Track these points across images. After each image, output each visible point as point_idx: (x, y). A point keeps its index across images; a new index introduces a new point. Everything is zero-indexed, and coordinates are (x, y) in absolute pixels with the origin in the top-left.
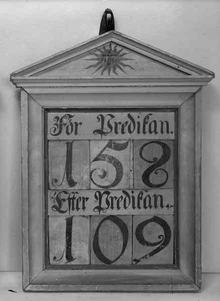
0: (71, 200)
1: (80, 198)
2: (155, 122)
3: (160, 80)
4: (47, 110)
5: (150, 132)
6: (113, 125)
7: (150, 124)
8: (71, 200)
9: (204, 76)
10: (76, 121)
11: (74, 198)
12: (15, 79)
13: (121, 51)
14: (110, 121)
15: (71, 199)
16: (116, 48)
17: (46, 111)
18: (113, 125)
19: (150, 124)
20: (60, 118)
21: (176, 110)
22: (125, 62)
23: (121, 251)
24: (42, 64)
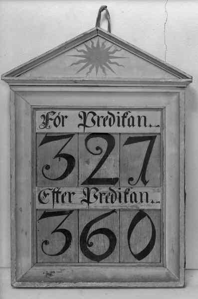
0: (55, 194)
1: (66, 193)
2: (133, 117)
3: (166, 83)
4: (35, 109)
5: (129, 125)
6: (96, 121)
7: (129, 120)
8: (55, 194)
9: (184, 80)
10: (63, 115)
11: (58, 192)
12: (15, 76)
13: (109, 48)
14: (94, 118)
15: (55, 192)
16: (105, 44)
17: (34, 111)
18: (96, 121)
19: (129, 120)
20: (46, 115)
21: (161, 110)
22: (112, 60)
23: (53, 178)
24: (58, 51)
